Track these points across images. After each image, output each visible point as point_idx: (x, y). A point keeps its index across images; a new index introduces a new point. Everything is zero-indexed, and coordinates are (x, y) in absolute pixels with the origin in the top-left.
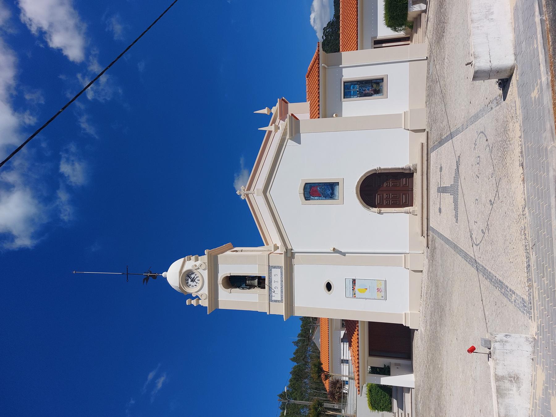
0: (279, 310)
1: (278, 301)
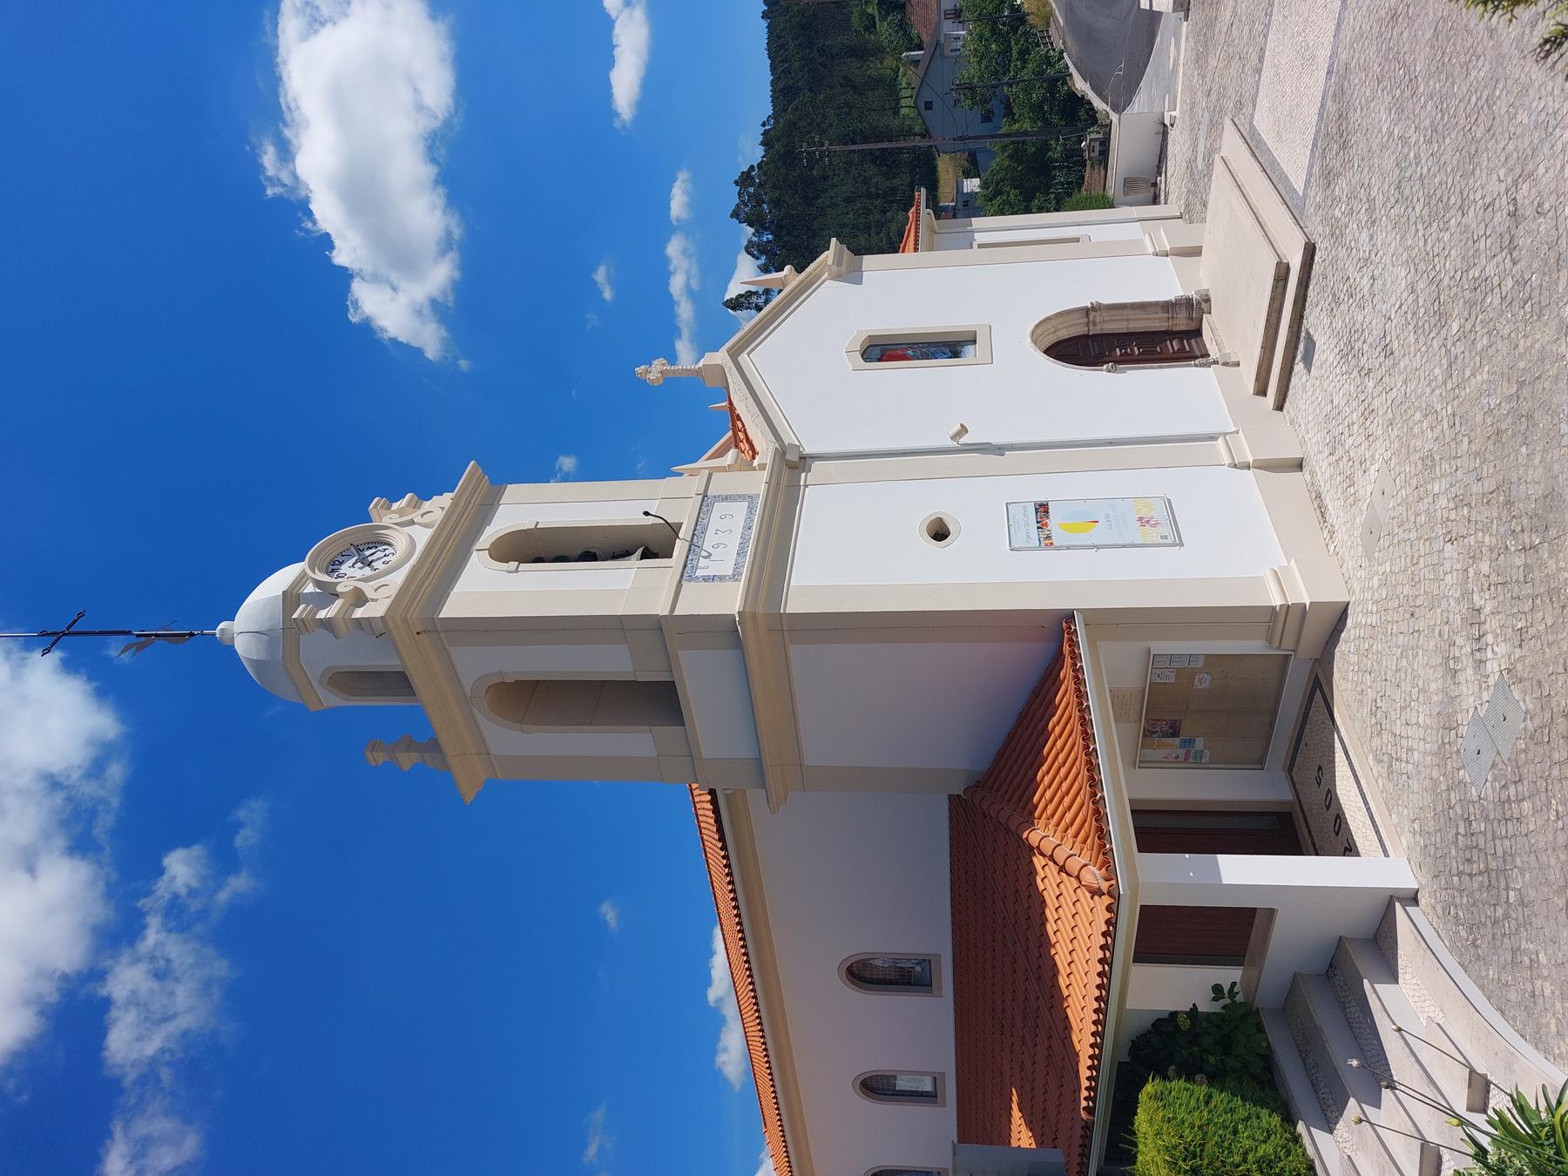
1: (722, 578)
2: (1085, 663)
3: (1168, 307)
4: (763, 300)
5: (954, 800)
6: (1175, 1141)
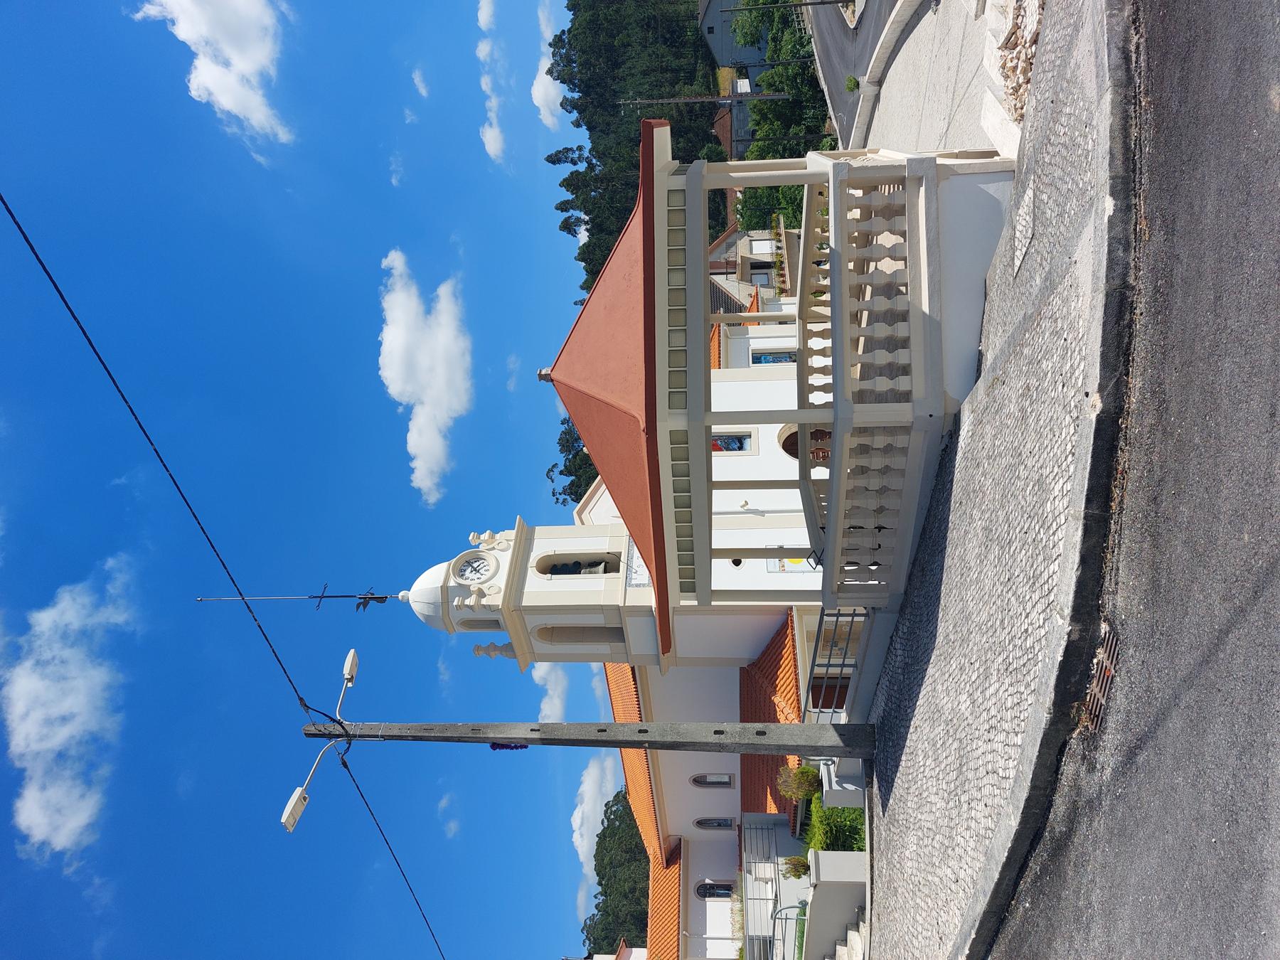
4: (577, 156)
5: (742, 669)
6: (822, 814)
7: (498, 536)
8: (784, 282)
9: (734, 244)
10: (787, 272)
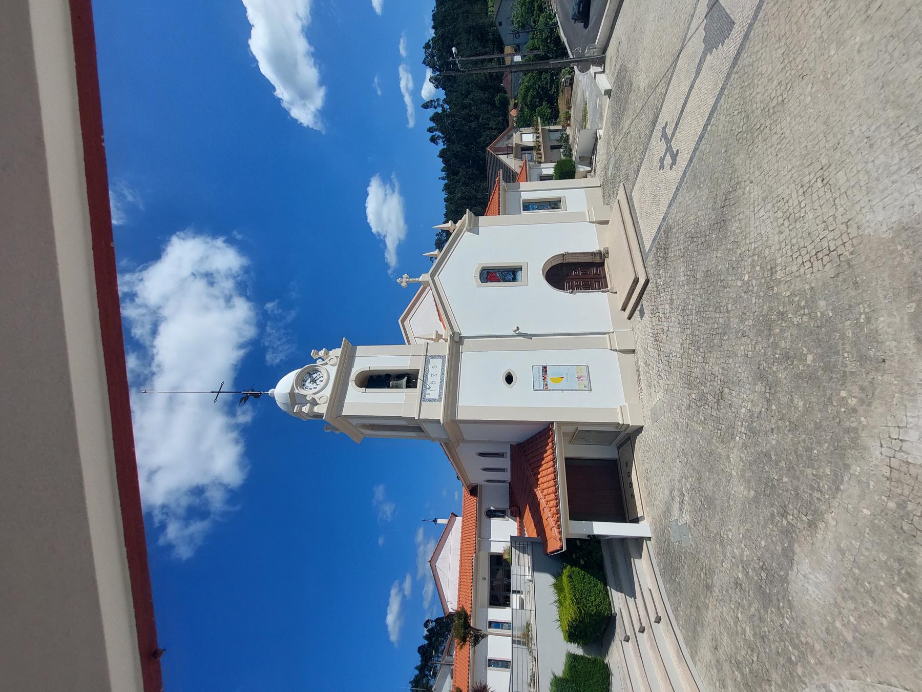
0: (436, 412)
1: (435, 400)
2: (556, 446)
3: (593, 254)
7: (331, 353)
8: (541, 158)
9: (512, 135)
10: (542, 151)
